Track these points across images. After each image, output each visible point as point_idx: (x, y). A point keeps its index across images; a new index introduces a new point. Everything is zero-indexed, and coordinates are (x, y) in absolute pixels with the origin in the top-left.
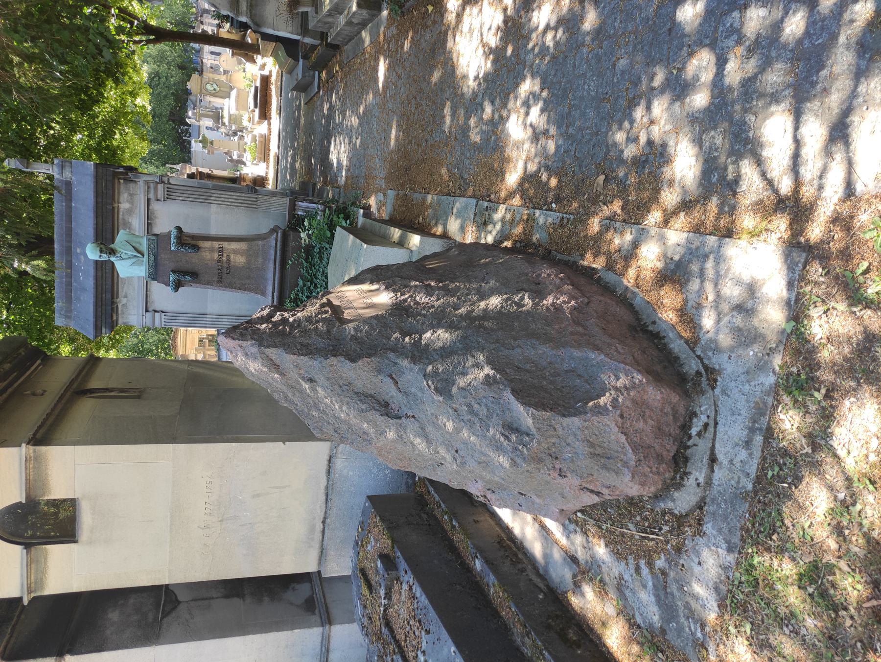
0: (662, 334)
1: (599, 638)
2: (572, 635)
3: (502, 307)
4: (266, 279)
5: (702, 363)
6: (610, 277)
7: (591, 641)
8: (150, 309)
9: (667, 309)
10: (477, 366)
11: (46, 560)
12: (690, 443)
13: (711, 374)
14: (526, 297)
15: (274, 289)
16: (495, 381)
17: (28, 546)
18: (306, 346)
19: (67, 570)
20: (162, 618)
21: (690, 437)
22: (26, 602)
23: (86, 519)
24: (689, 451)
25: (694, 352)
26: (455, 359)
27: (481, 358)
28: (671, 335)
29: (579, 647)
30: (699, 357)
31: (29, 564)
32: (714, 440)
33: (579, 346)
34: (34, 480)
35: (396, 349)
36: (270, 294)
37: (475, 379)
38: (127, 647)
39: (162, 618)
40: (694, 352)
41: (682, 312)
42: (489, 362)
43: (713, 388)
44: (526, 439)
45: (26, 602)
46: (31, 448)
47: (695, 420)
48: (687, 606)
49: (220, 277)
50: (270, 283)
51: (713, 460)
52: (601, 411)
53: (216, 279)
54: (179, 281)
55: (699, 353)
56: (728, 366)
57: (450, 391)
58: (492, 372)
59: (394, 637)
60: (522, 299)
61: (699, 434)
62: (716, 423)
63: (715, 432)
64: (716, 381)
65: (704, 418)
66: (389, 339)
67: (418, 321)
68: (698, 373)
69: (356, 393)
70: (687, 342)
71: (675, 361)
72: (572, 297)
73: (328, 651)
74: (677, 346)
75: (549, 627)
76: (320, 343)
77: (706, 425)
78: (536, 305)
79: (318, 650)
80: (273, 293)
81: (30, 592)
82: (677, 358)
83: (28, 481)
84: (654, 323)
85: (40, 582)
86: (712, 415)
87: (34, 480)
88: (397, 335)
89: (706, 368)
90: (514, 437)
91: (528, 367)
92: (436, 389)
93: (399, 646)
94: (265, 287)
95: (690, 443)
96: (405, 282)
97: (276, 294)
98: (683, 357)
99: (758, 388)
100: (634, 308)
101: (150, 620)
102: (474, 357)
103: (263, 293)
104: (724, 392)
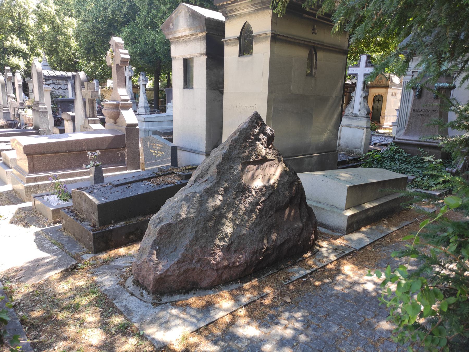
0: (186, 295)
1: (127, 246)
2: (131, 237)
3: (223, 232)
4: (414, 136)
5: (163, 303)
6: (235, 286)
7: (128, 243)
8: (414, 73)
9: (194, 301)
10: (189, 213)
11: (234, 45)
12: (141, 289)
13: (155, 305)
14: (225, 243)
15: (407, 140)
16: (177, 218)
17: (239, 38)
18: (235, 147)
19: (231, 52)
20: (219, 90)
21: (143, 290)
22: (223, 40)
23: (246, 59)
24: (139, 287)
25: (170, 302)
26: (197, 205)
27: (191, 215)
28: (183, 297)
29: (126, 238)
30: (166, 303)
31: (233, 39)
32: (137, 297)
33: (183, 255)
34: (260, 37)
35: (218, 183)
36: (404, 138)
37: (183, 211)
38: (207, 78)
39: (219, 90)
40: (170, 302)
41: (188, 305)
42: (187, 218)
43: (152, 303)
44: (155, 225)
45: (223, 40)
46: (270, 35)
47: (147, 293)
48: (106, 273)
49: (417, 111)
50: (411, 138)
51: (132, 295)
52: (151, 254)
53: (416, 108)
54: (416, 88)
55: (168, 304)
56: (152, 311)
57: (185, 201)
58: (182, 218)
59: (162, 175)
60: (225, 241)
61: (142, 293)
62: (141, 300)
63: (138, 298)
64: (153, 305)
65: (145, 296)
66: (226, 182)
67: (232, 195)
68: (161, 300)
69: (210, 166)
70: (175, 301)
71: (170, 294)
72: (217, 264)
73: (198, 153)
74: (177, 297)
75: (137, 229)
76: (235, 153)
77: (142, 296)
78: (218, 246)
79: (199, 150)
80: (404, 139)
81: (226, 41)
82: (172, 295)
83: (259, 35)
84: (194, 294)
85: (228, 44)
86: (144, 300)
87: (260, 37)
88: (226, 185)
89: (160, 304)
90: (157, 221)
91: (182, 233)
92: (187, 196)
93: (158, 176)
94: (409, 135)
95: (141, 289)
96: (267, 195)
97: (403, 141)
98: (171, 298)
99: (136, 316)
100: (208, 289)
101: (219, 86)
102: (194, 213)
103: (405, 134)
104: (147, 306)
